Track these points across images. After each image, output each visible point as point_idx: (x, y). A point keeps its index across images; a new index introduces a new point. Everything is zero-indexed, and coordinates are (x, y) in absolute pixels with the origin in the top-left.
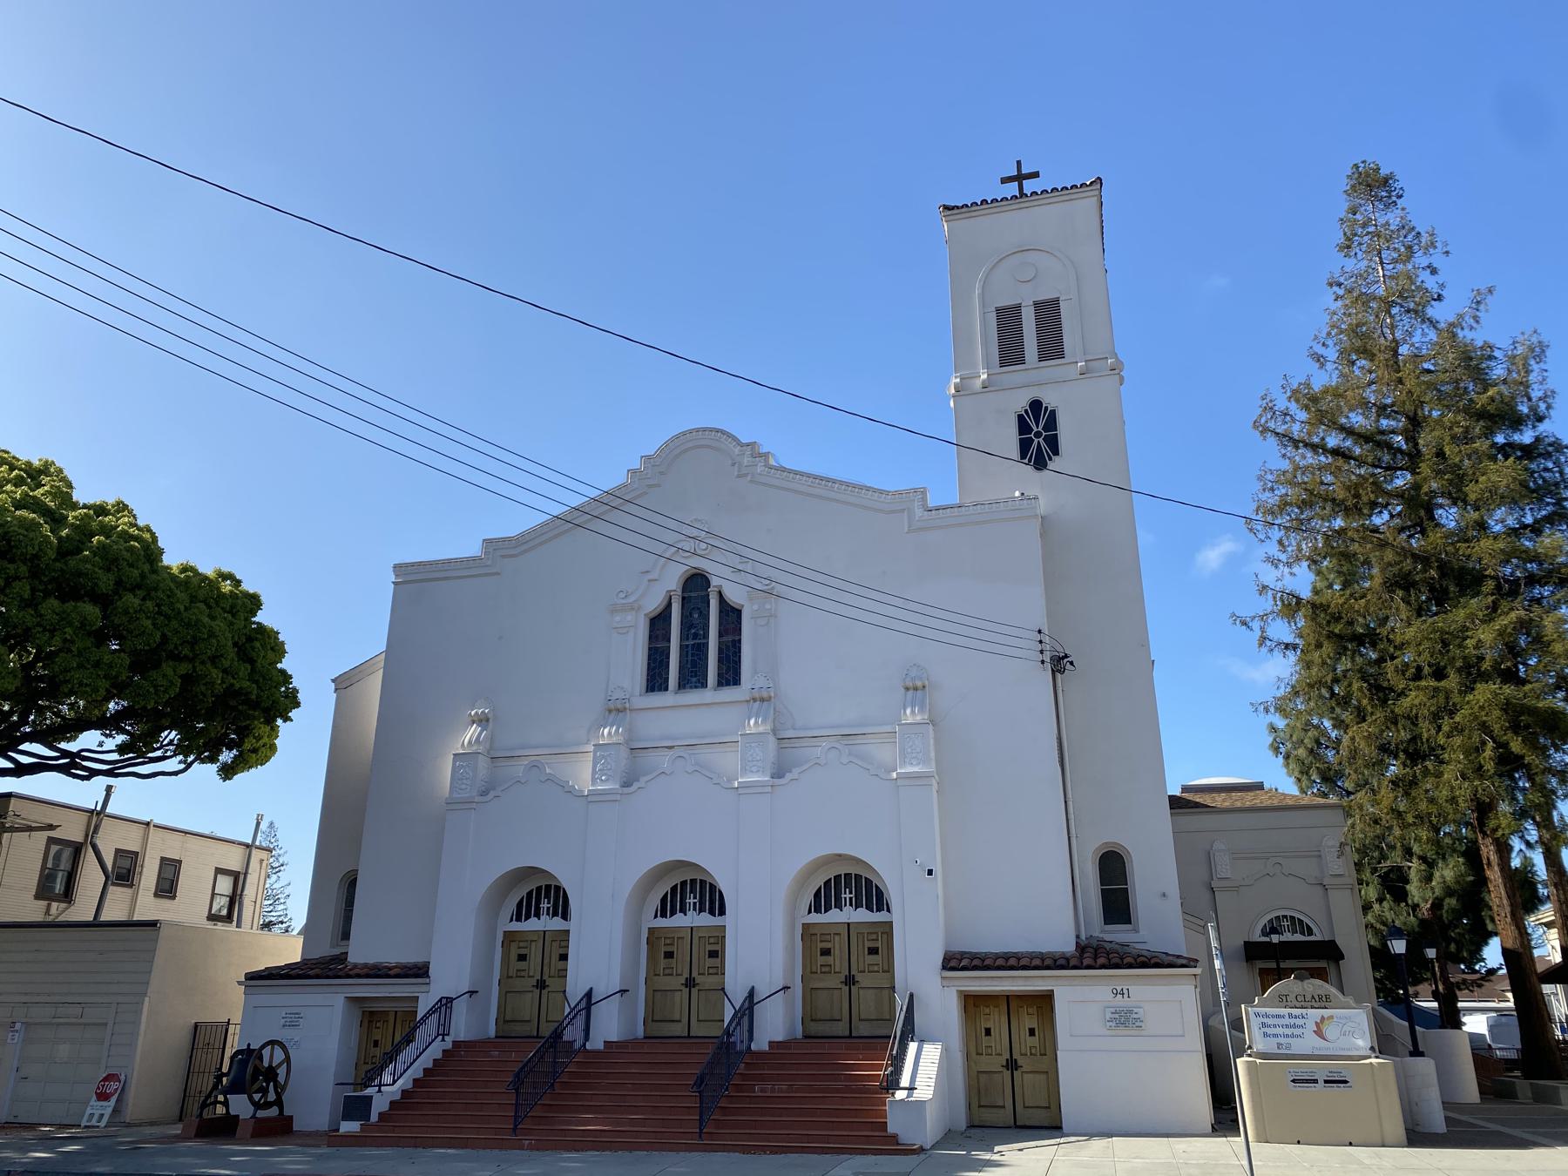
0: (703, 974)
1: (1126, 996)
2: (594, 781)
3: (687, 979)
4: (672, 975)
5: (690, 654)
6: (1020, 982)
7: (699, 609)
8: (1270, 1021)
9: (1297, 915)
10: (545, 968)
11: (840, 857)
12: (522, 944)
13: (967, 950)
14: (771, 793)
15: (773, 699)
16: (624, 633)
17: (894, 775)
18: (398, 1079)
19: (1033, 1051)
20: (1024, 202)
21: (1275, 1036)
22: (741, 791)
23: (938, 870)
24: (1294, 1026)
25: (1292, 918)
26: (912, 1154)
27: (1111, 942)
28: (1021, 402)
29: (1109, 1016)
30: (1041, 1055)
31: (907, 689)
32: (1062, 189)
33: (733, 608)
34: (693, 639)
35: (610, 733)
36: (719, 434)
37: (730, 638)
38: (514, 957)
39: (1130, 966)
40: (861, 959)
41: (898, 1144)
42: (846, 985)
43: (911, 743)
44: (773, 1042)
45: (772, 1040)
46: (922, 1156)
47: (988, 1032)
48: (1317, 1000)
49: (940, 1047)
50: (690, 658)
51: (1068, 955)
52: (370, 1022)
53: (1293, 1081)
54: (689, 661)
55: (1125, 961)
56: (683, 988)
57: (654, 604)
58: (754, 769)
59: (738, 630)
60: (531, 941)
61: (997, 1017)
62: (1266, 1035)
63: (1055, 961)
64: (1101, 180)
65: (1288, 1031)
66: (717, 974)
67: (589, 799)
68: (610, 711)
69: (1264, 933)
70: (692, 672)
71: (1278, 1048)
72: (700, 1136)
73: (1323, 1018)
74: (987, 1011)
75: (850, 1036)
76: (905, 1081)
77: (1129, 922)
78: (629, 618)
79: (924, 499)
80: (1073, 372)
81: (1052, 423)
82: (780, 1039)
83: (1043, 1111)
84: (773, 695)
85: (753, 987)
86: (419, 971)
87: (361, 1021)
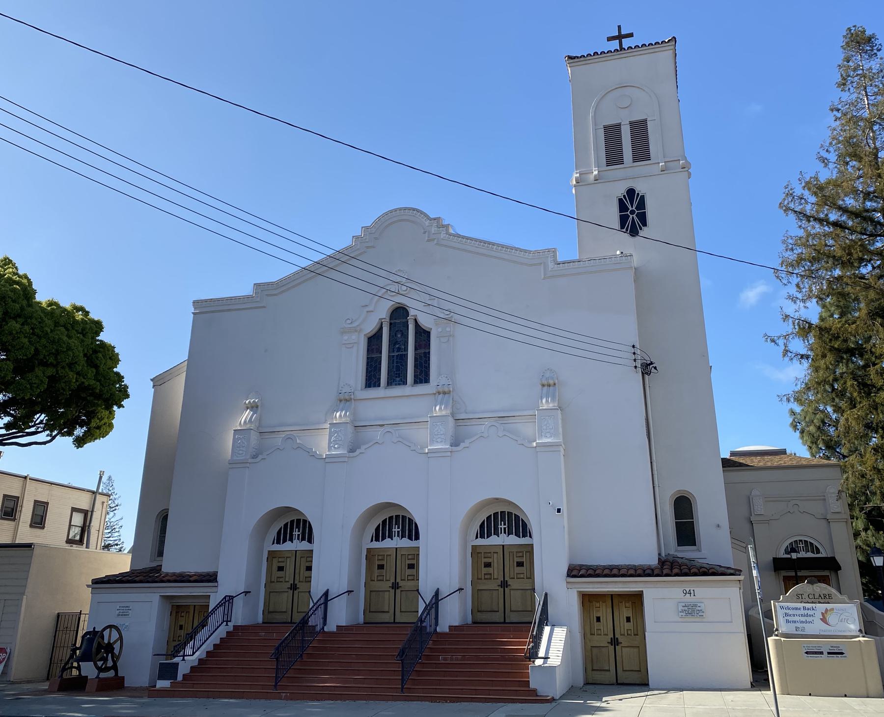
0: (404, 580)
1: (692, 594)
2: (330, 449)
4: (383, 580)
6: (620, 585)
7: (401, 331)
8: (790, 612)
9: (809, 540)
10: (297, 576)
11: (497, 500)
12: (280, 560)
15: (451, 393)
16: (350, 348)
17: (534, 444)
18: (196, 651)
20: (623, 54)
21: (794, 622)
22: (429, 455)
23: (564, 509)
24: (807, 615)
25: (806, 542)
27: (682, 558)
28: (621, 190)
29: (680, 608)
31: (543, 385)
35: (340, 416)
36: (415, 212)
37: (422, 351)
38: (275, 568)
39: (695, 575)
40: (512, 569)
42: (502, 587)
43: (546, 422)
44: (452, 626)
47: (598, 619)
48: (823, 598)
49: (566, 629)
50: (395, 364)
51: (653, 567)
53: (807, 653)
55: (692, 571)
56: (390, 589)
57: (370, 327)
58: (439, 440)
59: (428, 345)
62: (788, 621)
63: (644, 571)
64: (675, 39)
65: (803, 619)
66: (413, 580)
67: (327, 460)
68: (341, 401)
69: (787, 552)
70: (396, 374)
71: (796, 630)
73: (827, 610)
74: (598, 605)
75: (505, 623)
76: (542, 653)
78: (354, 337)
79: (555, 256)
80: (656, 169)
81: (642, 204)
82: (457, 624)
84: (451, 389)
86: (211, 578)
87: (171, 612)
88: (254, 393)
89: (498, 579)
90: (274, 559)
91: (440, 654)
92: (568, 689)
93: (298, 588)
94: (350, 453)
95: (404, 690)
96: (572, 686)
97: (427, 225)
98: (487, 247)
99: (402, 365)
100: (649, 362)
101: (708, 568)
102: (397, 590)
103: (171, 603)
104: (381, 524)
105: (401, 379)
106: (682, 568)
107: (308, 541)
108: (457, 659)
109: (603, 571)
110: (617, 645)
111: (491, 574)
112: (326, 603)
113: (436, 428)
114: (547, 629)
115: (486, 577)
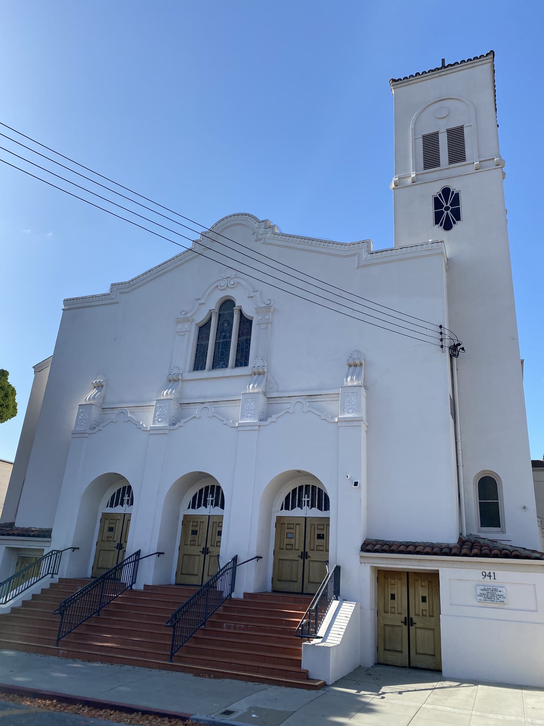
0: (214, 546)
1: (492, 577)
2: (154, 422)
3: (204, 548)
4: (195, 545)
5: (220, 348)
6: (415, 563)
7: (228, 321)
11: (299, 473)
12: (111, 521)
13: (381, 539)
14: (258, 430)
15: (266, 373)
17: (336, 420)
18: (9, 600)
19: (424, 613)
20: (444, 72)
22: (239, 429)
23: (363, 483)
26: (313, 689)
27: (484, 539)
28: (436, 189)
29: (479, 592)
30: (430, 616)
31: (350, 366)
32: (468, 61)
33: (247, 319)
34: (223, 339)
35: (167, 393)
36: (247, 216)
37: (245, 338)
38: (106, 528)
39: (496, 556)
40: (312, 541)
41: (308, 679)
42: (302, 558)
43: (349, 399)
44: (247, 593)
45: (246, 592)
46: (321, 692)
47: (393, 597)
49: (354, 605)
50: (220, 350)
51: (451, 546)
52: (22, 563)
54: (220, 352)
55: (493, 552)
56: (201, 554)
57: (201, 317)
58: (249, 415)
59: (249, 333)
60: (117, 519)
61: (399, 586)
63: (442, 549)
64: (493, 53)
67: (151, 432)
68: (170, 381)
70: (221, 358)
72: (171, 658)
74: (393, 582)
75: (302, 593)
76: (321, 632)
77: (498, 525)
78: (186, 326)
79: (369, 247)
80: (471, 169)
81: (456, 200)
82: (251, 591)
83: (430, 657)
84: (266, 371)
85: (237, 556)
86: (46, 534)
87: (17, 562)
88: (101, 375)
89: (299, 550)
90: (106, 521)
91: (225, 621)
92: (352, 670)
93: (123, 547)
94: (171, 426)
95: (173, 657)
96: (360, 666)
97: (256, 227)
98: (308, 243)
99: (226, 351)
100: (456, 343)
101: (511, 551)
102: (206, 555)
103: (18, 554)
104: (198, 493)
105: (224, 363)
106: (483, 548)
107: (318, 508)
108: (240, 628)
109: (399, 547)
110: (412, 626)
111: (293, 545)
112: (234, 569)
113: (247, 404)
114: (335, 604)
115: (288, 547)
